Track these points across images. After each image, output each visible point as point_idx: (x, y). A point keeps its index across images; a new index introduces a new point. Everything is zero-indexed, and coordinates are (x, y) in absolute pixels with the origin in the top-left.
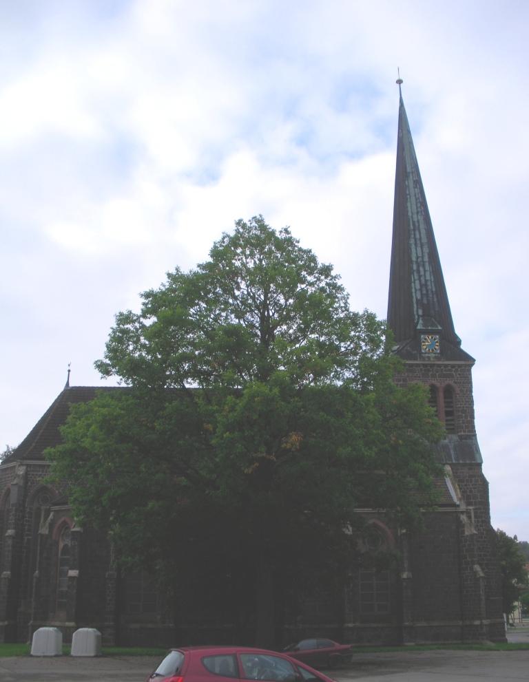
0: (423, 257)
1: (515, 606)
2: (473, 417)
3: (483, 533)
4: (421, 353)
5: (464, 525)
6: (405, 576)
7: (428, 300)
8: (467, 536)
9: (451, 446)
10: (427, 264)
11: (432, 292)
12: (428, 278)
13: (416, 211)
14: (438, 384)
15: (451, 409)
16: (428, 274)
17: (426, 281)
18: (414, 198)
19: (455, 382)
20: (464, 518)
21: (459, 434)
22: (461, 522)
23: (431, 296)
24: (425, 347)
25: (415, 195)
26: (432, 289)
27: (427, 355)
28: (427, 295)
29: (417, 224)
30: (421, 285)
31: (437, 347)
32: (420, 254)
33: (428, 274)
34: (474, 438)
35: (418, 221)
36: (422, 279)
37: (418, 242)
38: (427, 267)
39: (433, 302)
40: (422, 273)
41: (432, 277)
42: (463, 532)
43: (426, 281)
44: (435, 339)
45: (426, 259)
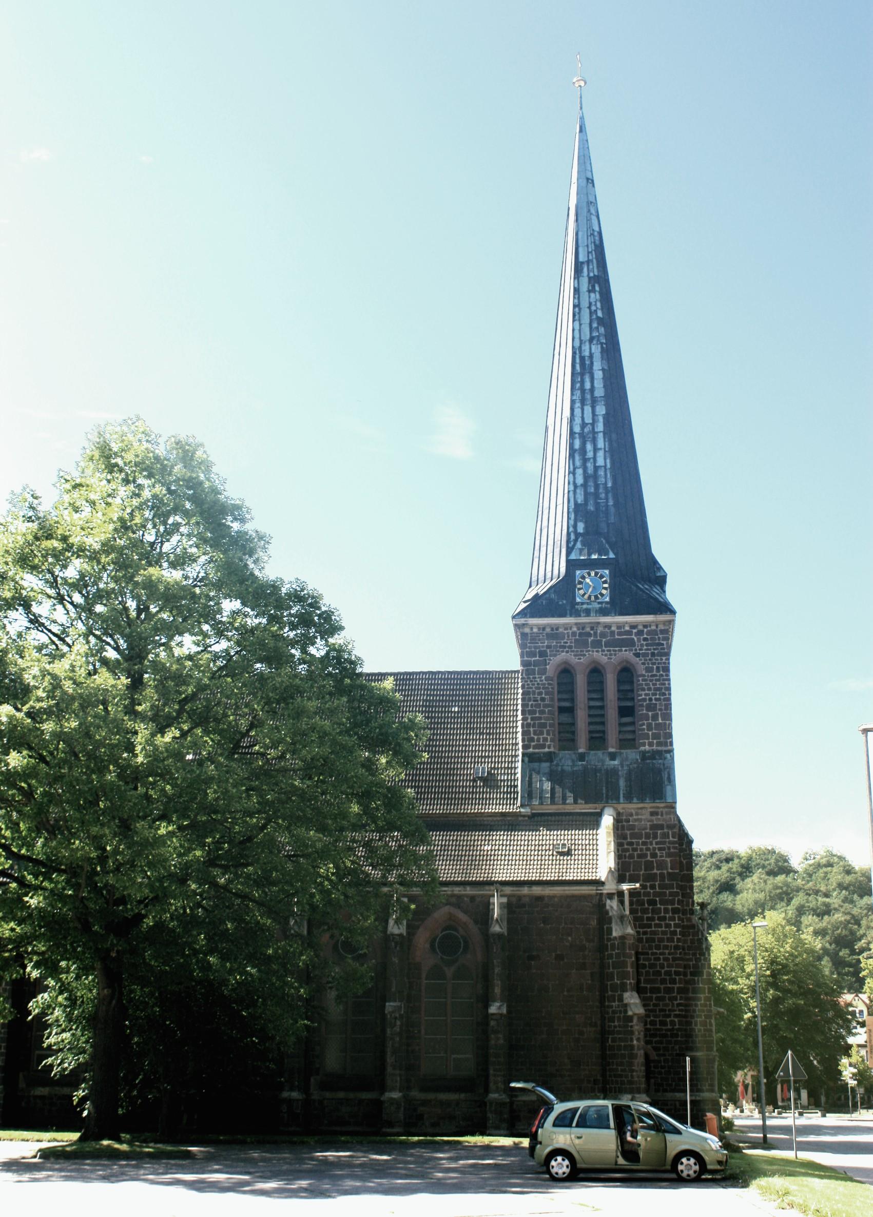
0: (593, 424)
1: (47, 987)
2: (668, 716)
3: (674, 933)
4: (573, 603)
5: (610, 918)
6: (493, 1009)
7: (597, 504)
8: (615, 938)
9: (623, 773)
10: (601, 436)
11: (606, 488)
12: (600, 462)
13: (588, 337)
14: (604, 659)
15: (629, 704)
16: (600, 454)
17: (596, 468)
18: (588, 311)
19: (637, 655)
20: (612, 905)
21: (642, 748)
22: (607, 912)
23: (603, 496)
24: (582, 592)
25: (589, 307)
26: (606, 483)
27: (585, 606)
28: (596, 495)
29: (587, 362)
30: (586, 477)
31: (604, 592)
32: (588, 420)
33: (600, 454)
34: (668, 756)
35: (591, 356)
36: (590, 465)
37: (588, 396)
38: (601, 443)
39: (607, 506)
40: (590, 454)
41: (608, 461)
42: (610, 931)
43: (596, 468)
44: (602, 577)
45: (600, 427)
